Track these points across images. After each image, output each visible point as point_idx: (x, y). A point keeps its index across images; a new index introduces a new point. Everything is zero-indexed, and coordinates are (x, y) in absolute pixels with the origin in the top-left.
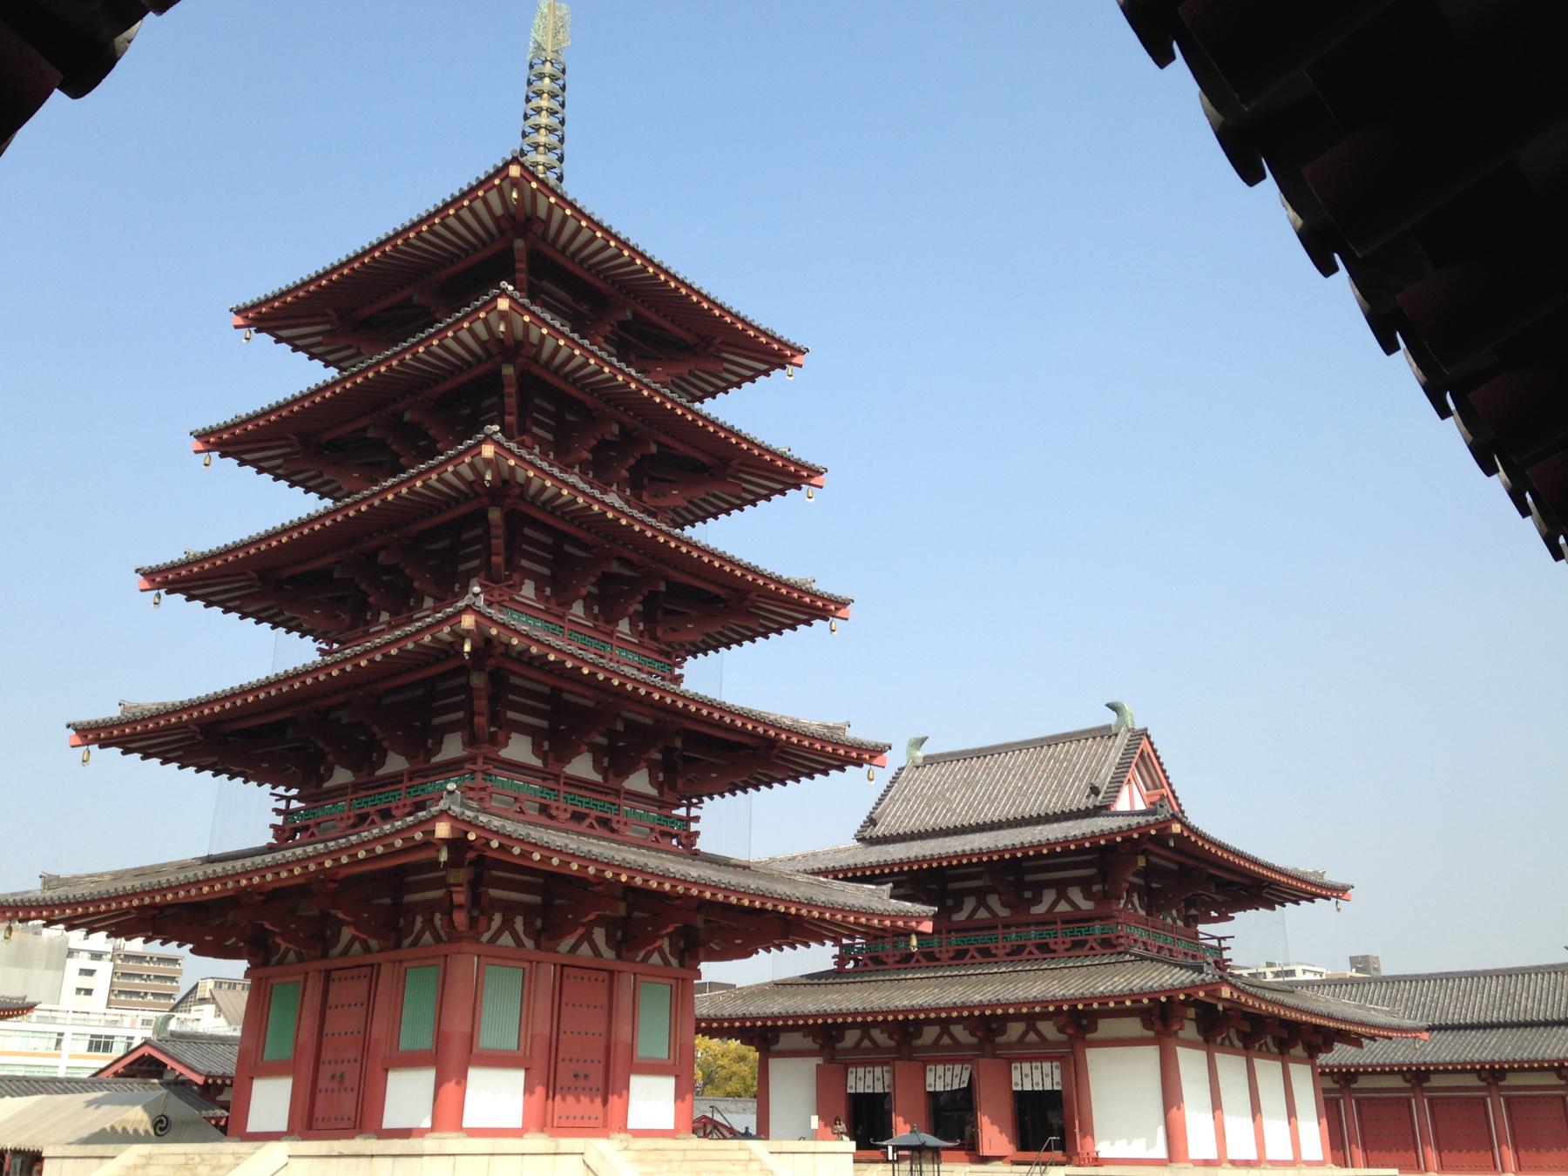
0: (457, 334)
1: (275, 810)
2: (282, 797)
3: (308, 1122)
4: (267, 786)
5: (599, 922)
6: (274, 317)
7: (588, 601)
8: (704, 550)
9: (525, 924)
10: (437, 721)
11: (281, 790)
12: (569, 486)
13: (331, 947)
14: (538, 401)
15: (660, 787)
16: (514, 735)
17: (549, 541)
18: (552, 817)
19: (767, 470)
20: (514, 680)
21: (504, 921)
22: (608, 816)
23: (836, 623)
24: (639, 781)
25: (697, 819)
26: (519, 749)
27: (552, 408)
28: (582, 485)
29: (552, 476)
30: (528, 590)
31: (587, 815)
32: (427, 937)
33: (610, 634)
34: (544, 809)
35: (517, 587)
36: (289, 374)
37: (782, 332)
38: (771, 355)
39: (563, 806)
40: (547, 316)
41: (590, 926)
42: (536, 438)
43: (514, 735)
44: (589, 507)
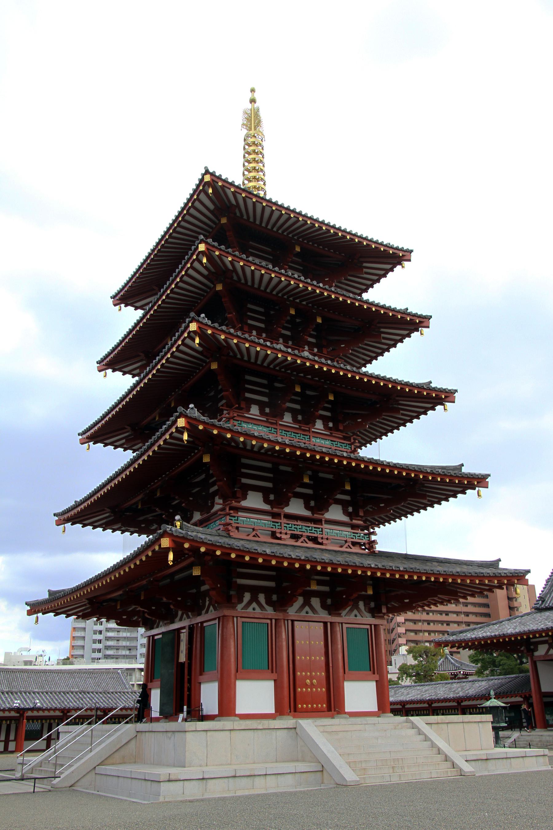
0: (214, 198)
8: (377, 377)
12: (279, 351)
14: (249, 306)
15: (350, 515)
16: (250, 493)
17: (265, 382)
19: (395, 323)
20: (244, 461)
22: (315, 535)
23: (406, 263)
25: (374, 533)
26: (254, 501)
27: (262, 310)
30: (255, 410)
31: (302, 536)
33: (309, 431)
34: (273, 535)
35: (248, 410)
37: (396, 243)
38: (392, 258)
39: (283, 531)
40: (264, 263)
43: (250, 493)
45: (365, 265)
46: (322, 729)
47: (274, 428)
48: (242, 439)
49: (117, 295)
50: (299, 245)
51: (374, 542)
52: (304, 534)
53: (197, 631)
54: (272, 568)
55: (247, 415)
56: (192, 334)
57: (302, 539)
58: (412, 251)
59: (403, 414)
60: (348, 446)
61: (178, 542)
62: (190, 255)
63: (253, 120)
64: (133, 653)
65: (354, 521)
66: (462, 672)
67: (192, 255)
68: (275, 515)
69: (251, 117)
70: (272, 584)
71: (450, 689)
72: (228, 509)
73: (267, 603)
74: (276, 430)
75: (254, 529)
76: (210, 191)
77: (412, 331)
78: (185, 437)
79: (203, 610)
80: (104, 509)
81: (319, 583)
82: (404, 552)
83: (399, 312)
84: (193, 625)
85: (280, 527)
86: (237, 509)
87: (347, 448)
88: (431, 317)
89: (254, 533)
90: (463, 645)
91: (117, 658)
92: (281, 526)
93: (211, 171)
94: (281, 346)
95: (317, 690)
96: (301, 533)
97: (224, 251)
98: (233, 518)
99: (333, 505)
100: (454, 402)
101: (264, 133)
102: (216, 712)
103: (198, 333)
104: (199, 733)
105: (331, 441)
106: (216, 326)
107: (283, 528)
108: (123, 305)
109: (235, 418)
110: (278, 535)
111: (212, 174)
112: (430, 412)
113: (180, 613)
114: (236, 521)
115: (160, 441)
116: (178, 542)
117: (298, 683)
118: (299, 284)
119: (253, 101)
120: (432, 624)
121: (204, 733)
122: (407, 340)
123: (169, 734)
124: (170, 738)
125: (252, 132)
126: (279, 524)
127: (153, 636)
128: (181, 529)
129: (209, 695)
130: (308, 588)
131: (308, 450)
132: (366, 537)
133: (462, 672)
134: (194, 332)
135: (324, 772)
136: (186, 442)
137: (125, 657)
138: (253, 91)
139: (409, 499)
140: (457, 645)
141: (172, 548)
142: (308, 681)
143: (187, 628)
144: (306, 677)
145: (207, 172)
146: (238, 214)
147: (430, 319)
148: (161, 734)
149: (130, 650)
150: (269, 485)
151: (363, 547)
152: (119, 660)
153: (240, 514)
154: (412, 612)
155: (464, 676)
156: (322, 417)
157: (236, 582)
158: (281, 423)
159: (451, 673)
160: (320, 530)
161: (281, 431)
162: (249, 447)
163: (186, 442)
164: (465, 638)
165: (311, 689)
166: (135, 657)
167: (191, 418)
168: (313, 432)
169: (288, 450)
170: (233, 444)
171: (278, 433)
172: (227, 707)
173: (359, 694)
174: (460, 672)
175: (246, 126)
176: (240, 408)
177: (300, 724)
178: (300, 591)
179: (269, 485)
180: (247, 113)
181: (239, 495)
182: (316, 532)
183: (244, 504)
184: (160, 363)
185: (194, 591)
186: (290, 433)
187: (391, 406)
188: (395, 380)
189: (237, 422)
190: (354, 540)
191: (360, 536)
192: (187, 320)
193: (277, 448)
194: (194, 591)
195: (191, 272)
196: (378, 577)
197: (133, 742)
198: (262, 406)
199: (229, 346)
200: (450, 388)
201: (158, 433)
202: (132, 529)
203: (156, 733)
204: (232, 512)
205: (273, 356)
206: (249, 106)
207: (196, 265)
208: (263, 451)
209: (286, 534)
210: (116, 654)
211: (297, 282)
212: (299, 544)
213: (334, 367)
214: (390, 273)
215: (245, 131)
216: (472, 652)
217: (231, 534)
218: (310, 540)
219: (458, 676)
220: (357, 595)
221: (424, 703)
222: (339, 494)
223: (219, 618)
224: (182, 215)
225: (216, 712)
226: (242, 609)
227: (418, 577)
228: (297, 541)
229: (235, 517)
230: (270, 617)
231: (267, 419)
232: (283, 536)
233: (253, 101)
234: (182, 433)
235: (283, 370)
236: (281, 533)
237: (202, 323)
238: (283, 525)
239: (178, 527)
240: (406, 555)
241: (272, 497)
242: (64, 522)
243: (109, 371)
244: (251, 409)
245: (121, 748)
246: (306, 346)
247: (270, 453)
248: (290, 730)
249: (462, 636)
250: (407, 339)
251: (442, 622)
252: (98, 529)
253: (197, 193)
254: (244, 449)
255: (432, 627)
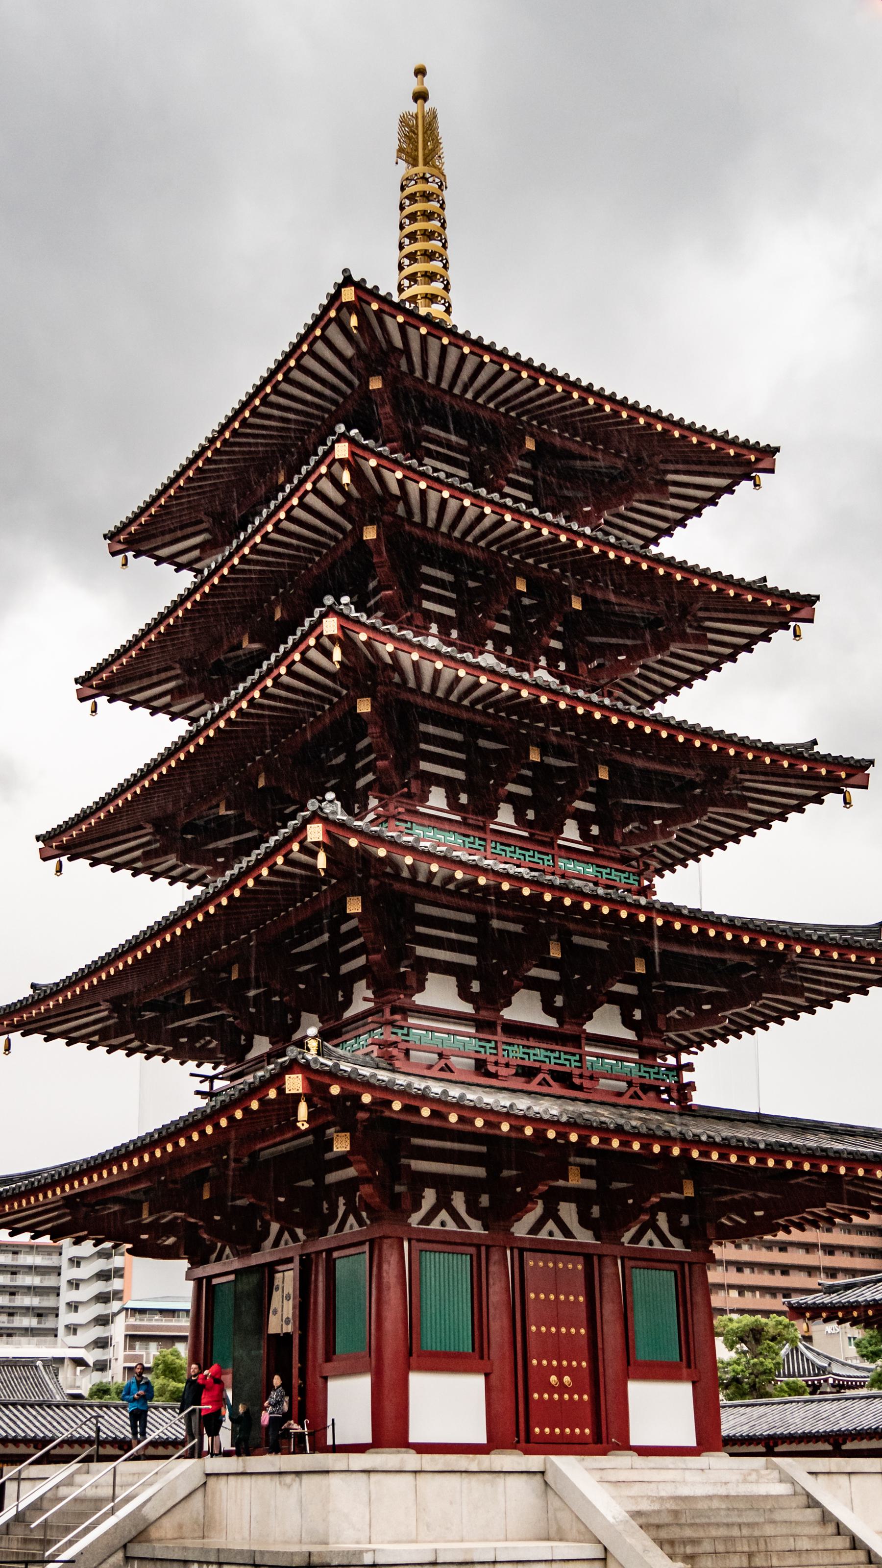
1: (197, 1093)
2: (206, 1078)
3: (516, 1425)
4: (191, 1065)
5: (664, 1205)
6: (136, 538)
7: (519, 804)
8: (692, 731)
9: (467, 1202)
10: (345, 968)
11: (207, 1069)
13: (278, 1243)
14: (426, 570)
16: (430, 976)
17: (457, 736)
18: (489, 1075)
20: (420, 908)
21: (545, 1209)
22: (566, 1069)
24: (606, 1022)
25: (690, 1067)
26: (439, 993)
27: (448, 577)
28: (502, 667)
29: (465, 663)
30: (437, 798)
32: (351, 1220)
33: (483, 828)
35: (424, 798)
36: (158, 587)
38: (741, 462)
39: (502, 1061)
41: (653, 1211)
42: (430, 616)
43: (430, 976)
44: (537, 700)
45: (670, 477)
46: (598, 1475)
47: (480, 839)
48: (409, 860)
49: (119, 530)
50: (532, 435)
51: (691, 1086)
52: (544, 1067)
53: (317, 1267)
54: (475, 1137)
55: (422, 810)
56: (326, 642)
57: (540, 1077)
58: (777, 450)
59: (752, 811)
60: (632, 877)
61: (318, 1080)
62: (312, 463)
63: (419, 140)
64: (49, 1323)
65: (645, 1040)
66: (831, 1381)
67: (318, 464)
68: (484, 1026)
69: (417, 134)
70: (480, 1172)
71: (818, 1413)
72: (387, 1011)
73: (469, 1212)
74: (483, 843)
75: (441, 1055)
76: (354, 321)
77: (774, 628)
78: (322, 861)
79: (331, 1224)
80: (114, 1004)
81: (586, 1172)
82: (754, 1109)
83: (749, 587)
84: (308, 1255)
85: (494, 1051)
86: (406, 1011)
87: (631, 881)
88: (818, 598)
89: (442, 1063)
90: (855, 1314)
91: (9, 1335)
92: (496, 1048)
93: (356, 278)
94: (487, 660)
95: (571, 1397)
96: (537, 1065)
97: (386, 458)
98: (400, 1032)
99: (523, 991)
100: (866, 787)
101: (446, 170)
102: (368, 1439)
103: (339, 638)
104: (354, 1475)
105: (598, 866)
106: (393, 631)
107: (501, 1053)
108: (130, 555)
109: (400, 817)
110: (492, 1069)
111: (360, 286)
112: (810, 807)
113: (275, 1227)
114: (557, 1061)
115: (258, 866)
116: (318, 1080)
117: (531, 1381)
118: (540, 529)
119: (421, 96)
120: (747, 1271)
121: (364, 1476)
122: (760, 647)
123: (288, 1479)
124: (289, 1486)
125: (420, 169)
126: (493, 1045)
127: (209, 1278)
128: (318, 1054)
129: (349, 1402)
130: (561, 1183)
131: (565, 889)
132: (671, 1074)
133: (831, 1381)
134: (331, 637)
135: (609, 1560)
136: (323, 874)
137: (28, 1332)
138: (420, 72)
139: (764, 995)
140: (840, 1314)
141: (305, 1095)
142: (553, 1379)
143: (297, 1260)
144: (551, 1370)
145: (348, 280)
146: (404, 367)
147: (814, 603)
148: (267, 1478)
149: (40, 1315)
150: (470, 960)
151: (665, 1096)
152: (15, 1339)
153: (411, 1021)
154: (733, 1242)
155: (834, 1390)
156: (511, 798)
157: (409, 1166)
158: (492, 826)
159: (807, 1381)
160: (577, 1058)
161: (493, 845)
162: (422, 878)
163: (323, 874)
164: (860, 1299)
165: (561, 1396)
166: (54, 1332)
167: (334, 823)
168: (560, 846)
169: (526, 891)
170: (388, 870)
171: (488, 848)
172: (390, 1427)
173: (660, 1409)
174: (826, 1380)
175: (407, 154)
176: (409, 796)
177: (553, 1463)
178: (542, 1188)
179: (470, 960)
180: (408, 125)
181: (412, 981)
182: (567, 1063)
183: (419, 999)
184: (244, 697)
185: (310, 1183)
186: (512, 849)
187: (727, 792)
188: (742, 739)
189: (404, 825)
190: (646, 1081)
191: (658, 1073)
192: (317, 612)
193: (482, 881)
194: (310, 1183)
195: (311, 499)
196: (635, 1154)
197: (199, 1495)
198: (451, 787)
199: (396, 666)
200: (857, 757)
201: (257, 852)
202: (151, 1047)
203: (254, 1478)
204: (397, 1017)
205: (471, 679)
206: (413, 108)
207: (326, 486)
208: (451, 887)
209: (507, 1065)
210: (6, 1325)
211: (537, 524)
212: (533, 1086)
213: (617, 711)
214: (726, 497)
215: (403, 169)
216: (858, 1333)
217: (397, 1064)
218: (555, 1079)
219: (822, 1390)
220: (658, 1200)
221: (757, 1444)
222: (620, 981)
223: (372, 1242)
224: (285, 369)
225: (368, 1439)
226: (419, 1224)
227: (794, 1164)
228: (528, 1082)
229: (402, 1028)
230: (475, 1241)
231: (464, 818)
232: (502, 1071)
233: (421, 96)
234: (314, 855)
235: (491, 711)
236: (496, 1063)
237: (347, 618)
238: (501, 1047)
239: (313, 1051)
240: (759, 1114)
241: (475, 987)
242: (9, 1029)
243: (102, 700)
244: (431, 796)
245: (174, 1506)
246: (542, 658)
247: (465, 891)
248: (531, 1476)
249: (851, 1296)
250: (760, 643)
251: (771, 1268)
252: (79, 1044)
253: (322, 324)
254: (413, 881)
255: (747, 1278)
